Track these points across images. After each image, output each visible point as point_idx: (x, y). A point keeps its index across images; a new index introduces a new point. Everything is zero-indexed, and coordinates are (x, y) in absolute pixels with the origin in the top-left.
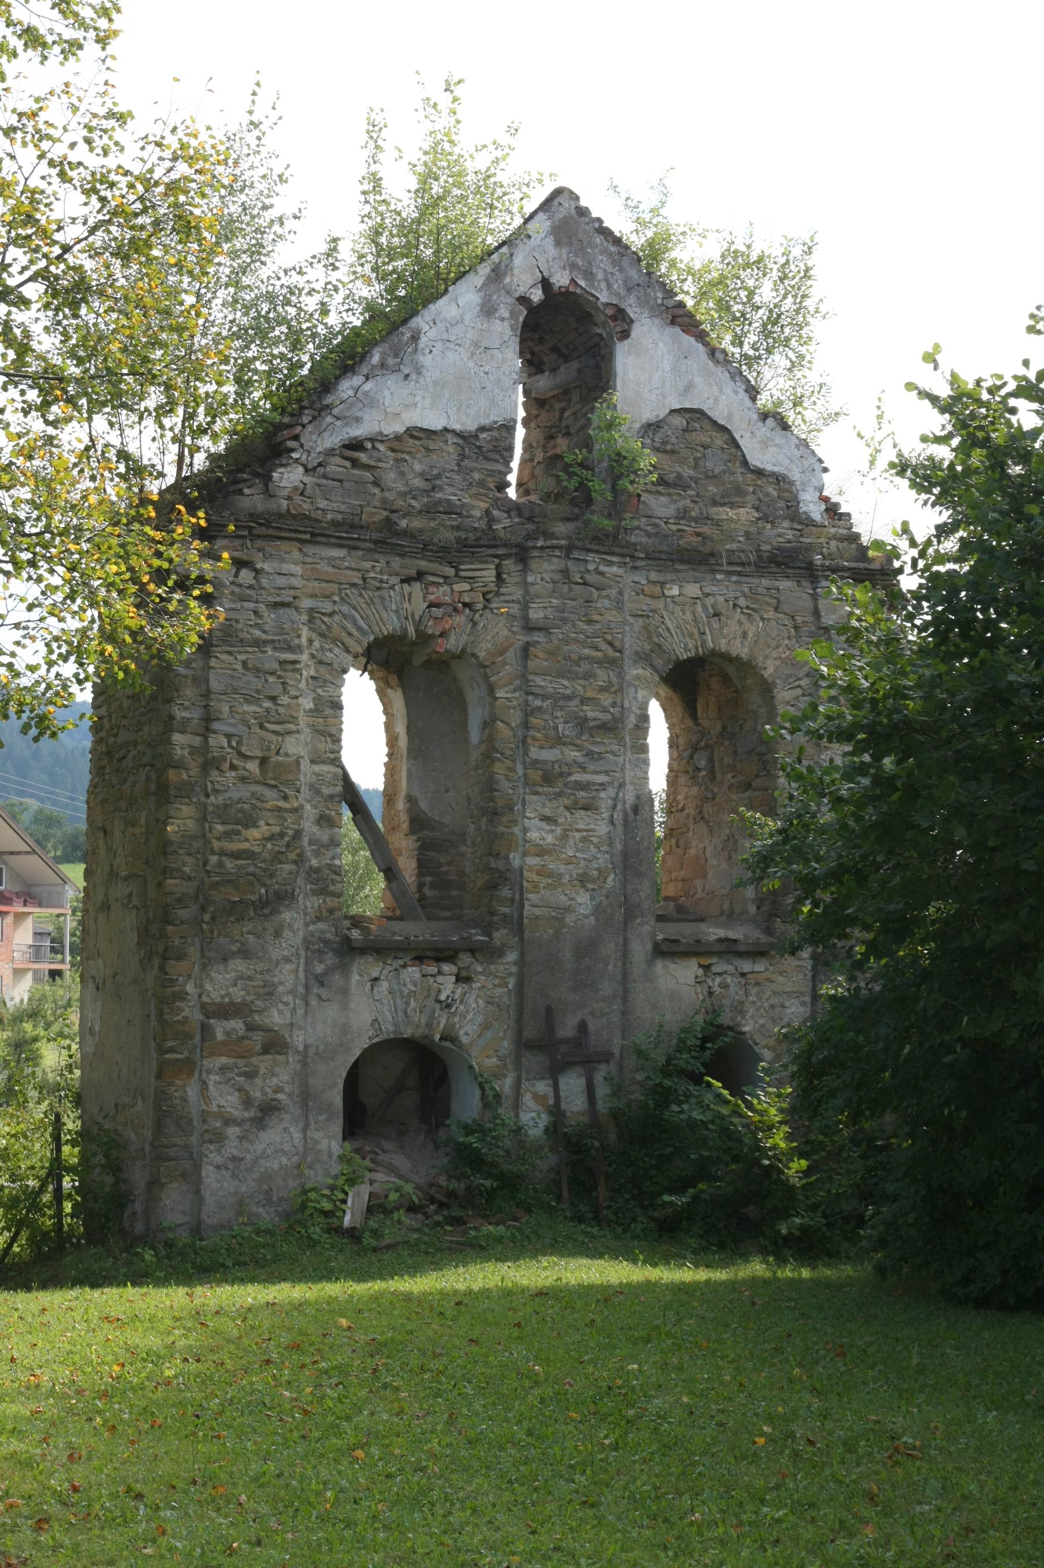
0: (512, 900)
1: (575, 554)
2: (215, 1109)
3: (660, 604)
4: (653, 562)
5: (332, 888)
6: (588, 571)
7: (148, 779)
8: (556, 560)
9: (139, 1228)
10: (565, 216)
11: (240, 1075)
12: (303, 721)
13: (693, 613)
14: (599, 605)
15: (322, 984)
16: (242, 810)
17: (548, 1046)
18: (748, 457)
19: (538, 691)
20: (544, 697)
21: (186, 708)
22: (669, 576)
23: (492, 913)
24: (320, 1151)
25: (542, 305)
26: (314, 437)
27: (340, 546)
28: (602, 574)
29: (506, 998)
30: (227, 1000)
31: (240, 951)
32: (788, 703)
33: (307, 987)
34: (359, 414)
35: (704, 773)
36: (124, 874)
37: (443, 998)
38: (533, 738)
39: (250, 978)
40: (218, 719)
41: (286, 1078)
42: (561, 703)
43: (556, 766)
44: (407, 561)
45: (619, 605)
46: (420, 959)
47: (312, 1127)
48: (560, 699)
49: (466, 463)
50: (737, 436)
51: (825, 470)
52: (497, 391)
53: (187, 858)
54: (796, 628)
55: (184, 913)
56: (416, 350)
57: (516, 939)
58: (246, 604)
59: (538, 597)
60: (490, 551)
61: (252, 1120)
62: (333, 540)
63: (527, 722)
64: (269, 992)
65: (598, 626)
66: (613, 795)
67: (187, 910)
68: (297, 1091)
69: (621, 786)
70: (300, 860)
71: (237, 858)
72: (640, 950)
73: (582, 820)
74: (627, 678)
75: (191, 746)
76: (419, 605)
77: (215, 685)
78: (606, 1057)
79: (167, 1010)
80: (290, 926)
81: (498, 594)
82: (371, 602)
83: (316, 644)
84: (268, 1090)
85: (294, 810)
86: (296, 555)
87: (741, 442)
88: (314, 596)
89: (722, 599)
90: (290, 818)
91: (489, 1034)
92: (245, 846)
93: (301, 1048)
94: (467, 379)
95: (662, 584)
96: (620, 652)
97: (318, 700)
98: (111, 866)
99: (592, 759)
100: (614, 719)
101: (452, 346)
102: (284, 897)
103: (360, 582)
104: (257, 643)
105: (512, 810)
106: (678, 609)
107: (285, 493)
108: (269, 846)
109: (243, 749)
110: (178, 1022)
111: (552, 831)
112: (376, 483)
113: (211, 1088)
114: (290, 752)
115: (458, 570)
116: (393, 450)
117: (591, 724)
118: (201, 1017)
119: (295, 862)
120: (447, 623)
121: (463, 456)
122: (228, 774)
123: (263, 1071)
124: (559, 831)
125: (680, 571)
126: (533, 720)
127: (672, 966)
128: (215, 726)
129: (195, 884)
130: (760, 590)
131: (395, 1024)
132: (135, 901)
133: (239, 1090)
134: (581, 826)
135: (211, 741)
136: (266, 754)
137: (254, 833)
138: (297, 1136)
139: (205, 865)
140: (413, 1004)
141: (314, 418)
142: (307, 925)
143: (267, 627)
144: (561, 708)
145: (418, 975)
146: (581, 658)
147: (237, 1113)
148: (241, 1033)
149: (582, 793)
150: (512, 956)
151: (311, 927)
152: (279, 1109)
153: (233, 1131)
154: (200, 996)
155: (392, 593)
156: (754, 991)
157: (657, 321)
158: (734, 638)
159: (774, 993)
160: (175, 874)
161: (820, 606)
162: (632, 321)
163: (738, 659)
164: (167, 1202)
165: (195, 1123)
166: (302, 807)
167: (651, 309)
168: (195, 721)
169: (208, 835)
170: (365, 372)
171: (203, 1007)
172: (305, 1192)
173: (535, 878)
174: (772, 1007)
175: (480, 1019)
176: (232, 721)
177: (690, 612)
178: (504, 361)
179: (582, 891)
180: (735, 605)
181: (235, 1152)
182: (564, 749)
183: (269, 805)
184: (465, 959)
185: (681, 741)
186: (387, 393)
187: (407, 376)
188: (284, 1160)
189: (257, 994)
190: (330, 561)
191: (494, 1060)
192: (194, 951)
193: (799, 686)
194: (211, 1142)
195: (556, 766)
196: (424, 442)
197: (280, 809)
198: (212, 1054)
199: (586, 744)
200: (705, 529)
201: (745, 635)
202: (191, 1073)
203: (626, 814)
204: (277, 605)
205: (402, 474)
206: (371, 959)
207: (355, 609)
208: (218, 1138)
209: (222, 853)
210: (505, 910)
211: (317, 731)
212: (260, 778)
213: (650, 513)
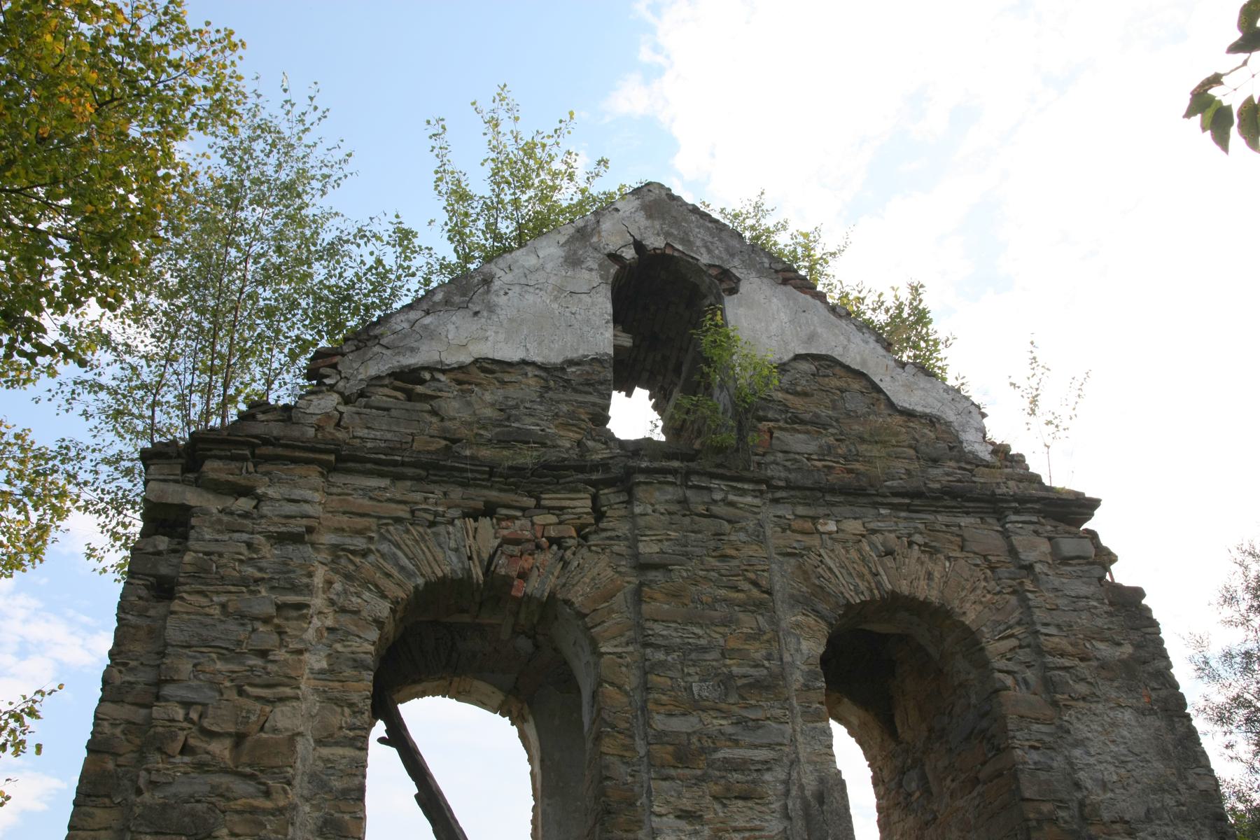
1: (695, 480)
3: (815, 541)
6: (715, 502)
8: (670, 489)
10: (657, 201)
13: (859, 551)
14: (733, 538)
18: (893, 399)
19: (660, 641)
20: (668, 649)
21: (132, 670)
22: (821, 511)
26: (355, 365)
27: (381, 475)
28: (732, 504)
32: (1003, 655)
34: (415, 345)
35: (917, 794)
38: (657, 702)
40: (172, 681)
42: (693, 656)
43: (694, 740)
44: (472, 492)
45: (759, 538)
50: (877, 380)
56: (488, 292)
58: (236, 536)
62: (369, 466)
63: (646, 683)
65: (735, 563)
66: (783, 776)
69: (794, 762)
73: (741, 815)
74: (784, 625)
75: (129, 722)
83: (338, 586)
85: (280, 811)
86: (316, 479)
89: (893, 535)
95: (814, 519)
96: (769, 592)
97: (333, 657)
101: (531, 290)
103: (408, 516)
104: (244, 581)
105: (632, 805)
106: (838, 547)
107: (314, 420)
109: (206, 723)
111: (696, 833)
112: (434, 413)
114: (279, 725)
115: (538, 499)
116: (459, 383)
117: (740, 682)
120: (527, 562)
125: (833, 504)
126: (653, 678)
134: (741, 823)
136: (242, 729)
141: (358, 349)
146: (715, 600)
155: (451, 529)
158: (918, 577)
161: (1015, 542)
162: (739, 280)
163: (926, 604)
166: (294, 807)
167: (758, 271)
170: (425, 308)
176: (194, 683)
177: (858, 556)
180: (910, 544)
182: (703, 715)
183: (238, 805)
185: (886, 773)
186: (451, 327)
190: (366, 492)
193: (1012, 636)
195: (694, 740)
196: (499, 375)
197: (254, 810)
199: (735, 709)
201: (929, 576)
203: (806, 806)
204: (281, 539)
205: (469, 404)
207: (398, 546)
212: (231, 764)
213: (785, 448)
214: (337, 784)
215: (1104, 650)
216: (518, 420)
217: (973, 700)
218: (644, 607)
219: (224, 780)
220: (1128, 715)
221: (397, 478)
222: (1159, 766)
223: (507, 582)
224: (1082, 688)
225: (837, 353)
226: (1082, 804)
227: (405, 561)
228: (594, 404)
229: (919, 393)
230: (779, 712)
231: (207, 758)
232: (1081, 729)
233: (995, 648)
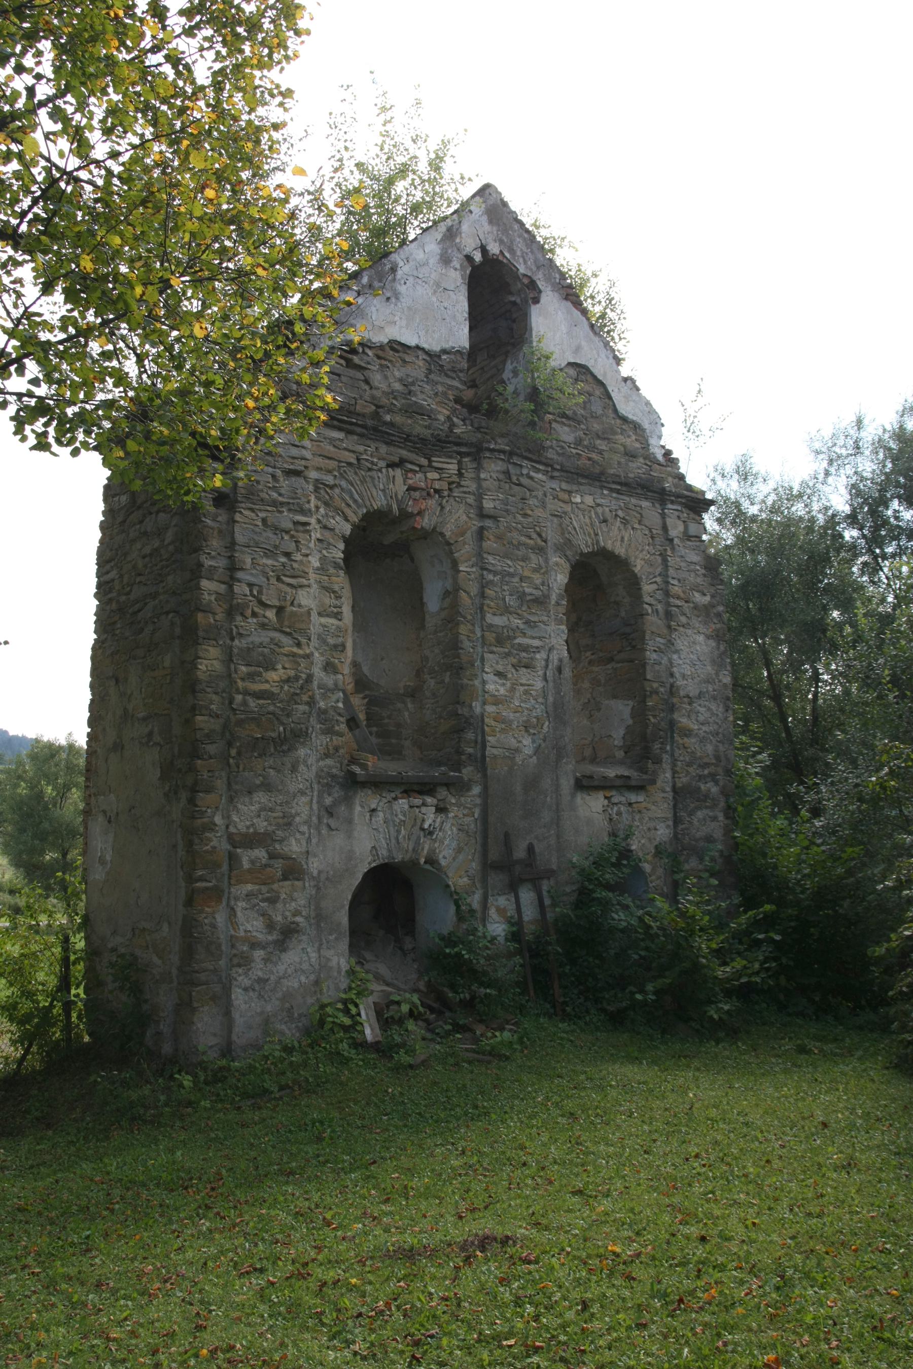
0: (476, 742)
1: (515, 459)
2: (242, 934)
3: (568, 508)
4: (565, 474)
5: (337, 728)
7: (172, 624)
8: (500, 463)
9: (167, 1049)
11: (263, 900)
12: (312, 576)
13: (590, 518)
15: (331, 814)
16: (263, 655)
17: (507, 865)
19: (490, 568)
20: (495, 573)
21: (213, 558)
22: (575, 487)
23: (459, 752)
24: (331, 968)
25: (482, 264)
27: (340, 429)
28: (531, 478)
29: (473, 826)
30: (251, 830)
31: (262, 784)
33: (319, 818)
36: (141, 715)
37: (426, 826)
38: (488, 606)
39: (271, 810)
40: (242, 569)
41: (303, 902)
44: (392, 449)
46: (407, 793)
47: (324, 946)
48: (505, 574)
49: (432, 376)
50: (610, 390)
51: (663, 425)
52: (453, 324)
53: (214, 697)
54: (652, 538)
55: (212, 749)
56: (394, 280)
57: (479, 775)
59: (489, 490)
60: (455, 448)
61: (276, 942)
64: (288, 823)
65: (530, 520)
67: (215, 746)
68: (313, 914)
70: (311, 703)
71: (259, 698)
72: (567, 784)
73: (524, 676)
74: (551, 563)
75: (217, 593)
76: (400, 488)
77: (240, 538)
78: (549, 874)
79: (197, 841)
80: (305, 761)
81: (459, 485)
82: (363, 481)
83: (322, 510)
84: (288, 913)
87: (613, 395)
88: (319, 469)
90: (303, 664)
91: (461, 857)
92: (266, 686)
93: (315, 873)
94: (429, 314)
96: (545, 541)
97: (323, 559)
98: (125, 709)
99: (530, 626)
100: (543, 595)
102: (300, 735)
103: (355, 462)
104: (274, 503)
108: (286, 688)
109: (264, 598)
110: (207, 852)
112: (367, 382)
113: (239, 914)
115: (430, 461)
116: (379, 357)
117: (529, 598)
118: (229, 847)
119: (308, 703)
121: (430, 371)
122: (250, 620)
123: (283, 896)
124: (508, 684)
125: (581, 484)
126: (488, 591)
127: (588, 798)
128: (240, 575)
129: (221, 721)
130: (630, 506)
131: (389, 851)
132: (157, 738)
133: (263, 915)
134: (524, 681)
135: (236, 589)
137: (273, 676)
138: (314, 955)
139: (231, 703)
140: (403, 832)
142: (318, 761)
143: (283, 491)
144: (507, 583)
145: (406, 807)
146: (520, 544)
147: (260, 936)
148: (264, 861)
149: (524, 654)
150: (476, 790)
151: (321, 763)
152: (298, 932)
153: (258, 954)
154: (227, 827)
156: (637, 817)
157: (556, 294)
158: (615, 540)
159: (650, 819)
160: (204, 712)
164: (199, 1025)
165: (223, 948)
166: (312, 654)
168: (221, 570)
169: (234, 675)
171: (230, 838)
172: (323, 1007)
173: (493, 723)
174: (649, 829)
175: (454, 844)
178: (457, 302)
179: (526, 735)
181: (260, 974)
183: (286, 650)
184: (442, 792)
187: (388, 299)
188: (303, 979)
189: (278, 825)
191: (465, 879)
192: (220, 784)
194: (239, 965)
196: (401, 354)
197: (294, 655)
198: (240, 882)
199: (525, 614)
200: (594, 456)
202: (219, 899)
204: (290, 473)
205: (386, 377)
206: (370, 792)
207: (352, 485)
208: (245, 962)
209: (246, 693)
210: (470, 750)
211: (323, 587)
212: (278, 626)
214: (331, 641)
215: (697, 597)
216: (415, 395)
217: (623, 614)
218: (484, 544)
219: (276, 635)
220: (701, 638)
221: (349, 432)
222: (709, 668)
223: (411, 515)
224: (683, 619)
225: (590, 364)
226: (672, 686)
227: (356, 496)
228: (457, 388)
229: (632, 404)
230: (545, 619)
231: (266, 621)
232: (680, 644)
233: (647, 588)
